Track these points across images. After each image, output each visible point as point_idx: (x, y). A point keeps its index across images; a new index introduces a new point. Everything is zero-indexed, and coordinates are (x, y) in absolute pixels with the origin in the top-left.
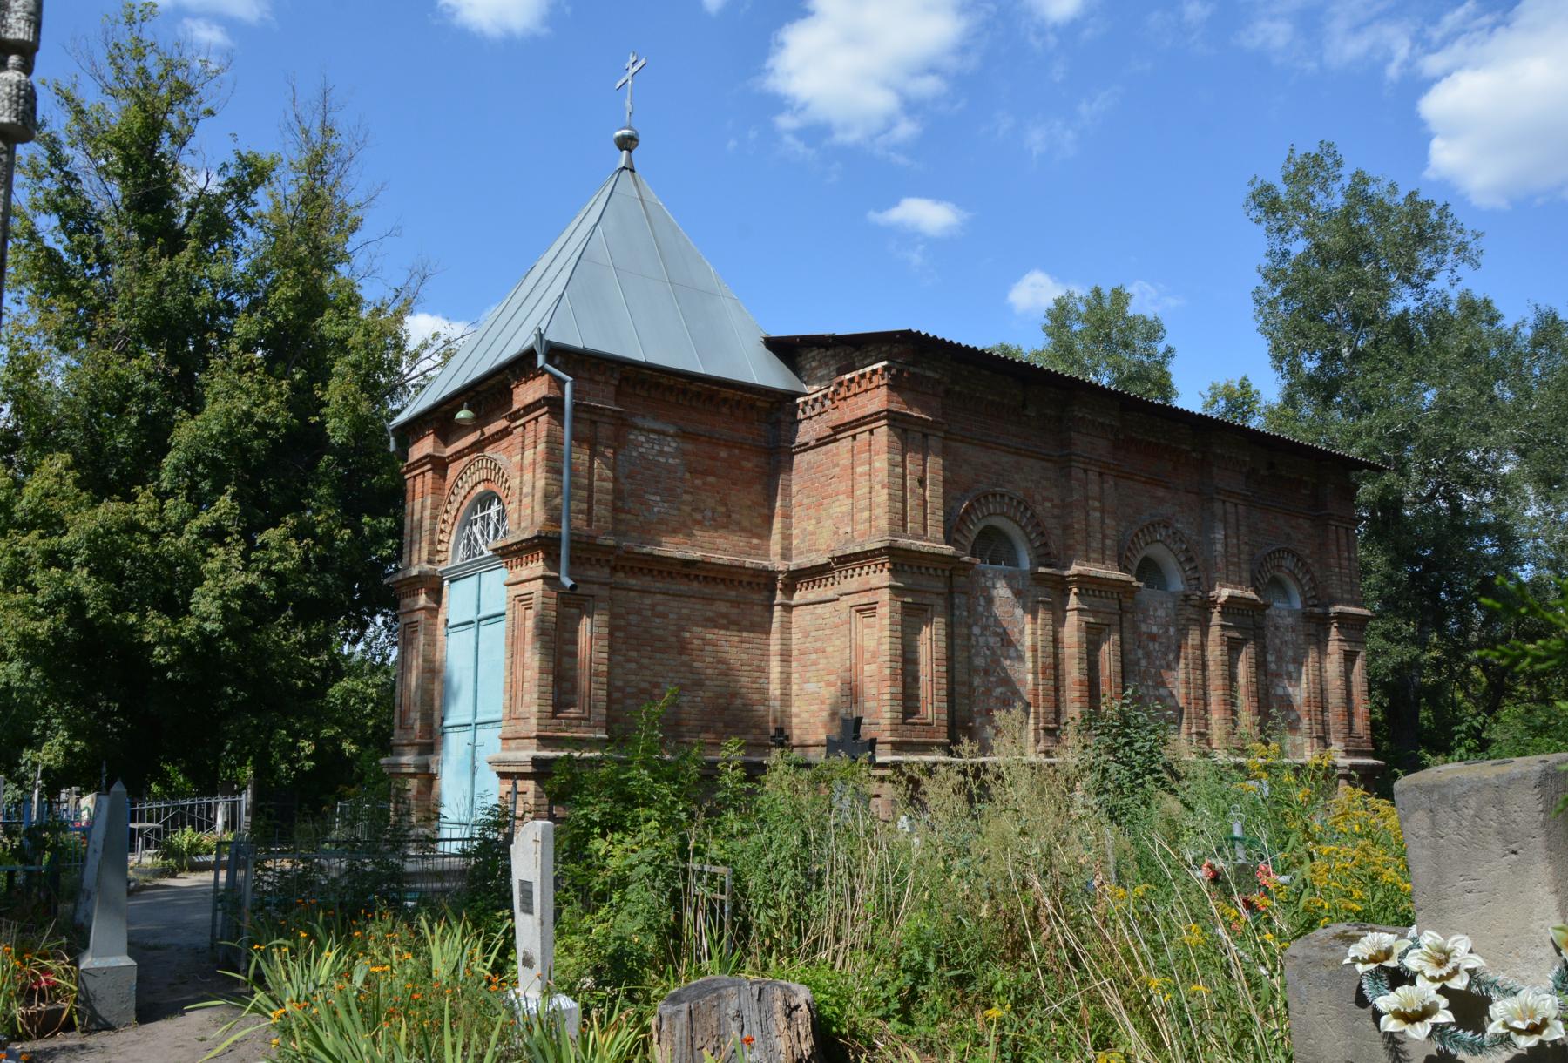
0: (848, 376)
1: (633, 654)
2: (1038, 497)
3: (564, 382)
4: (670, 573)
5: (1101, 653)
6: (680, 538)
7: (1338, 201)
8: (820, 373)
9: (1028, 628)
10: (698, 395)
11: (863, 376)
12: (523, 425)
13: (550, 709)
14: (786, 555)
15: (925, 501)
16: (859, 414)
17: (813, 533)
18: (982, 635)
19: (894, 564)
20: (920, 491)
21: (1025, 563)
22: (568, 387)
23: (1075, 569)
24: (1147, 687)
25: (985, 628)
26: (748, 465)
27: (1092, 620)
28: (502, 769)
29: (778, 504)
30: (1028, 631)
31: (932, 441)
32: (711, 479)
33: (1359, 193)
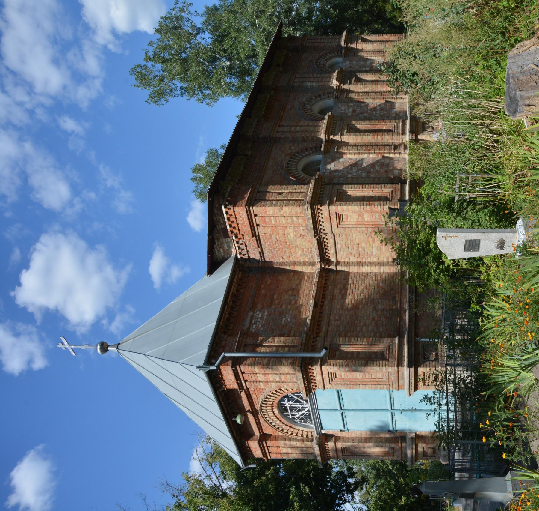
0: (228, 228)
1: (358, 328)
2: (289, 152)
3: (224, 356)
4: (320, 313)
5: (361, 128)
6: (303, 310)
7: (159, 66)
8: (226, 247)
9: (349, 156)
10: (234, 302)
11: (229, 219)
12: (245, 381)
13: (384, 362)
14: (313, 264)
15: (289, 192)
16: (247, 222)
17: (303, 250)
18: (352, 174)
19: (318, 204)
20: (284, 194)
21: (319, 157)
22: (228, 355)
23: (322, 136)
24: (376, 114)
25: (348, 173)
26: (269, 282)
27: (346, 131)
28: (413, 388)
29: (288, 268)
30: (350, 156)
31: (261, 189)
32: (275, 297)
33: (156, 58)
